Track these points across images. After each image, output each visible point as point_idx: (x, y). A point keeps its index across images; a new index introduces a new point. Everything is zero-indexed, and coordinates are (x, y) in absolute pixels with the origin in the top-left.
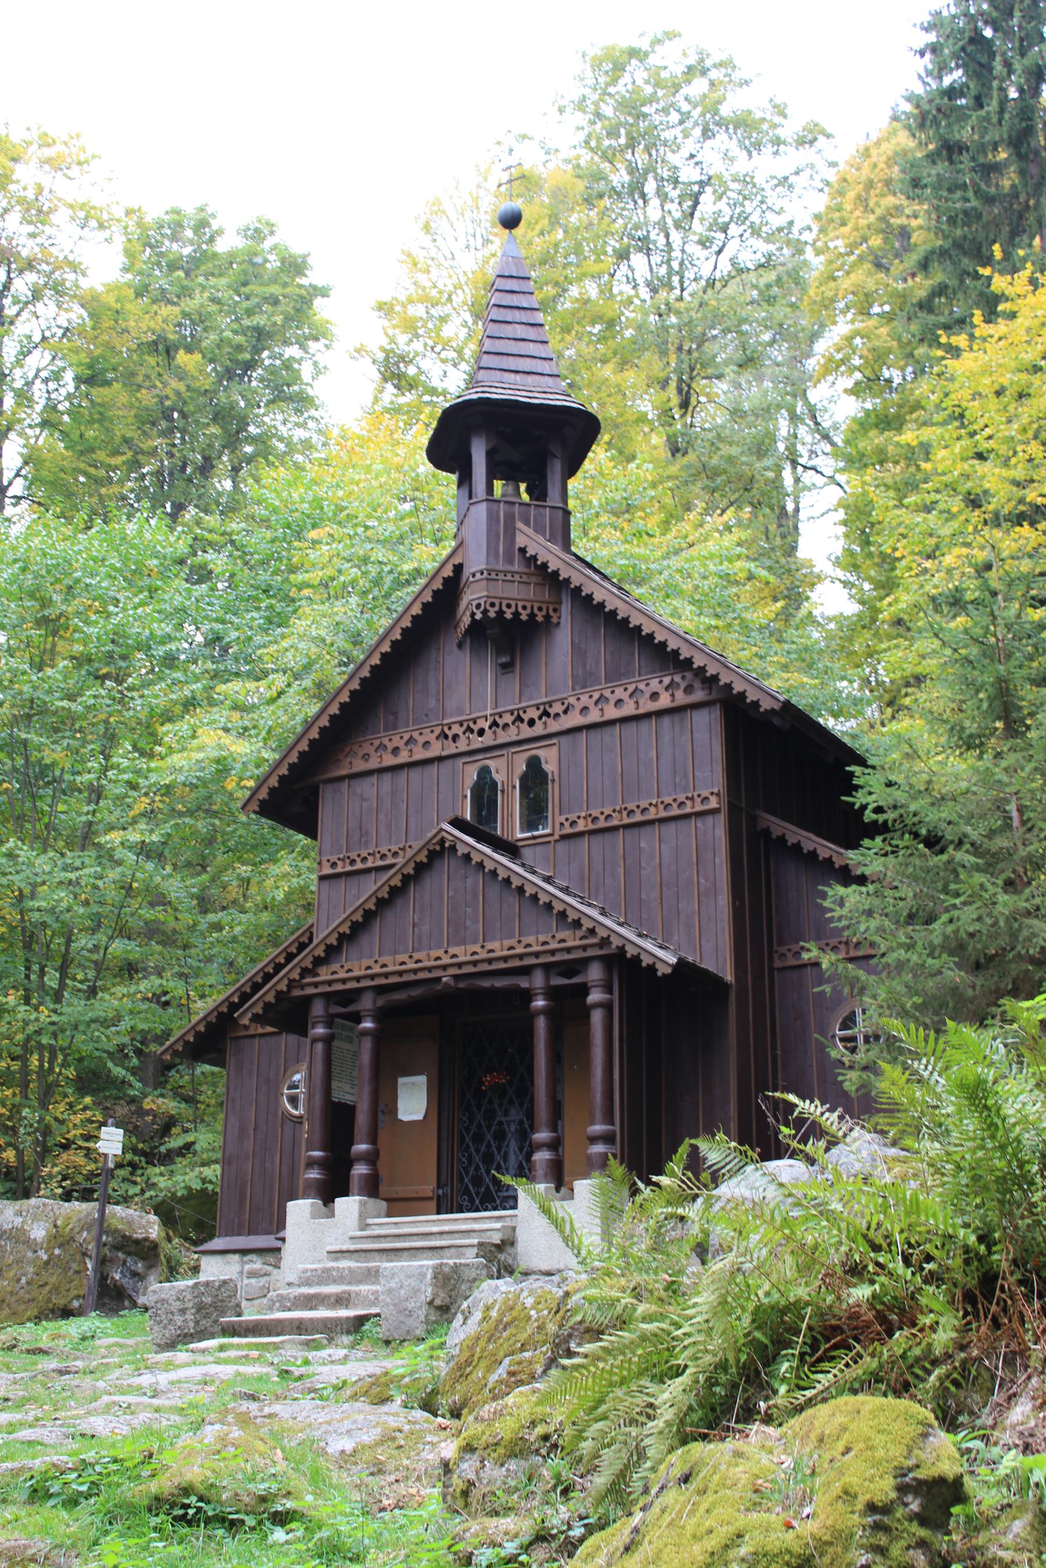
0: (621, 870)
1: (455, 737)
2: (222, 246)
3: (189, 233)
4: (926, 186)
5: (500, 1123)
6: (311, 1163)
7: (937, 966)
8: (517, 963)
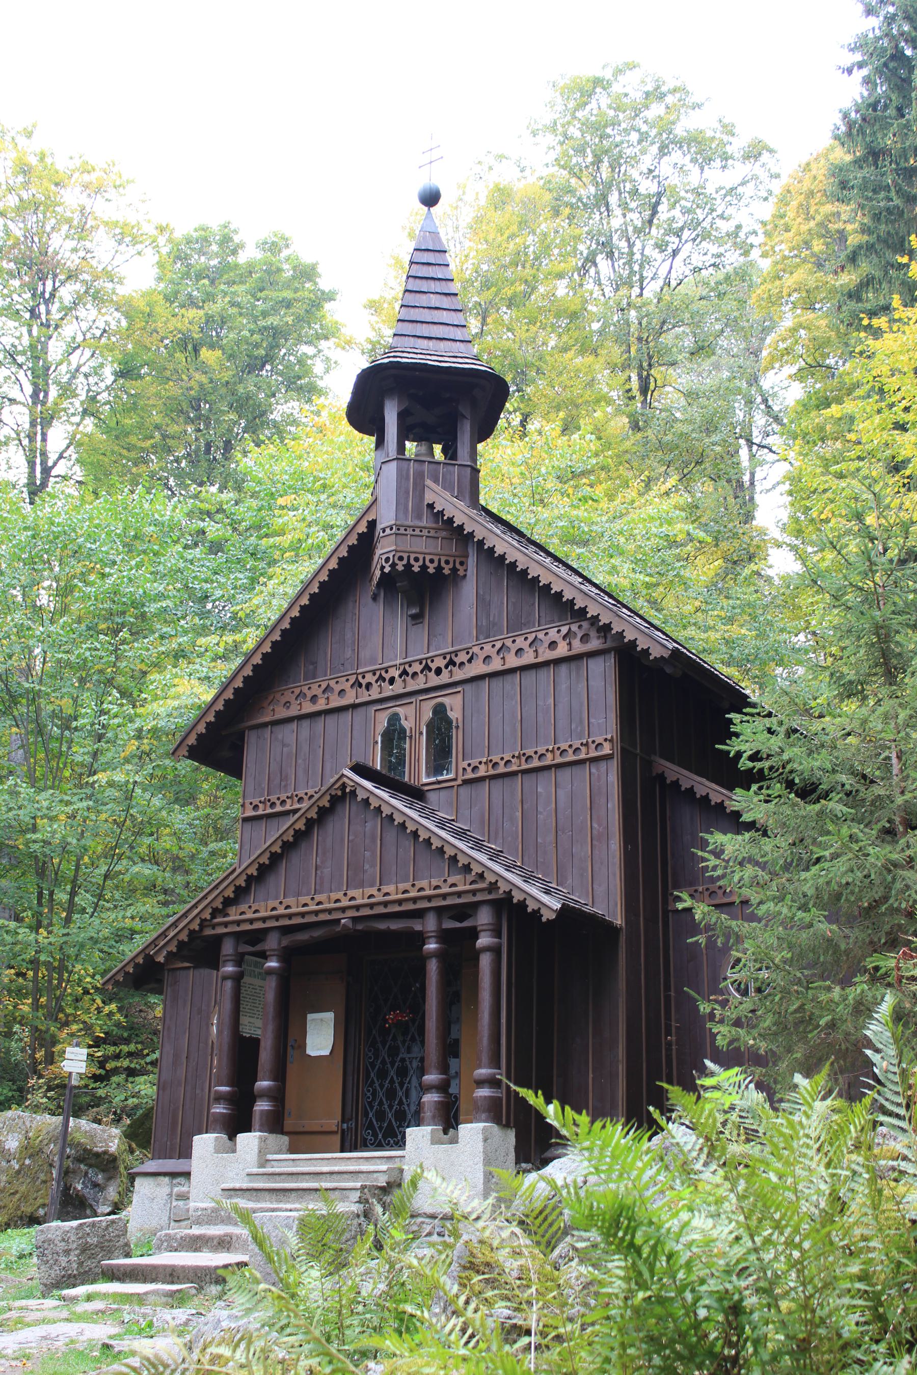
0: (519, 814)
1: (369, 686)
2: (242, 258)
3: (215, 248)
4: (853, 187)
5: (403, 1060)
6: (219, 1098)
7: (808, 920)
8: (411, 906)
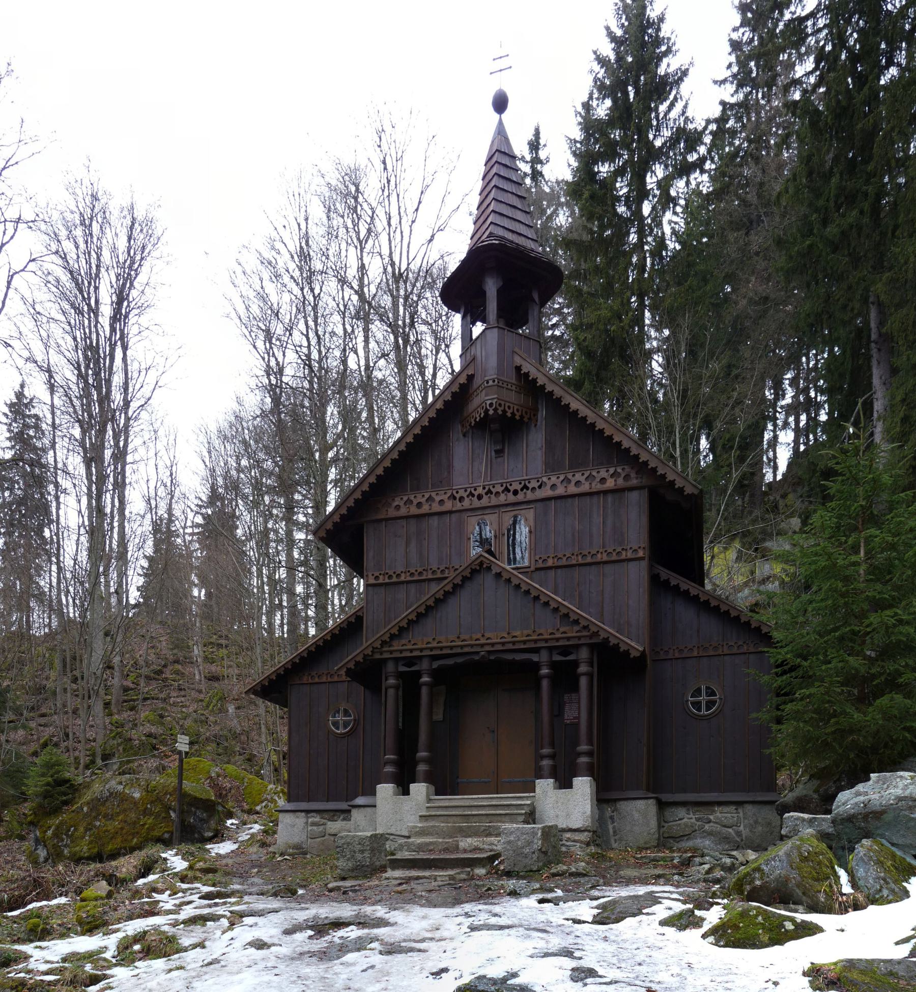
1: (461, 499)
8: (533, 645)
